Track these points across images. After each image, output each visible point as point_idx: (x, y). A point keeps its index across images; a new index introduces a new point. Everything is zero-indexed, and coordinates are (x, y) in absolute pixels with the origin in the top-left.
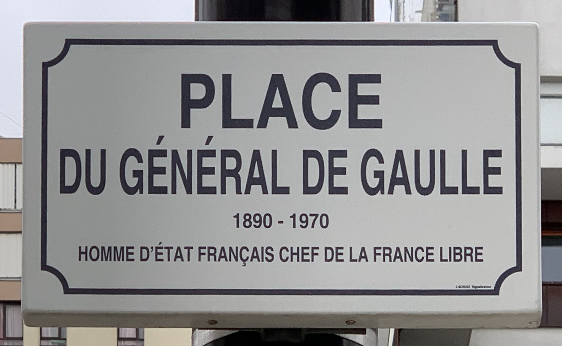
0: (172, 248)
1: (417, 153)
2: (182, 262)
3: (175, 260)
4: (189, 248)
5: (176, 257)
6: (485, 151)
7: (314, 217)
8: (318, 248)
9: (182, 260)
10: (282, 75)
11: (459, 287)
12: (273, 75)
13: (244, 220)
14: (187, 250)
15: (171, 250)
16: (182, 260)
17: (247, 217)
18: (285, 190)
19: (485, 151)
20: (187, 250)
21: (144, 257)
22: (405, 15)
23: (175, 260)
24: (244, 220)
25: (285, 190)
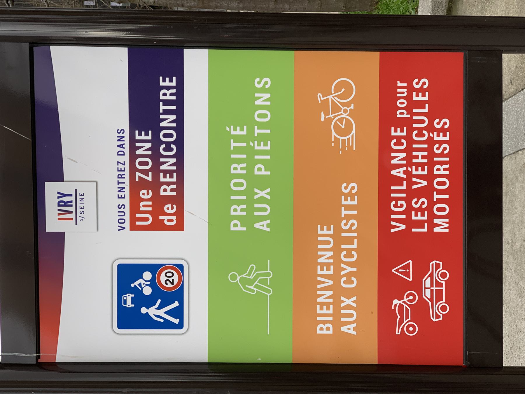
0: (118, 181)
1: (119, 216)
2: (125, 144)
3: (124, 148)
4: (119, 183)
5: (122, 147)
6: (125, 198)
7: (123, 163)
8: (118, 195)
9: (124, 144)
10: (403, 174)
11: (121, 190)
12: (267, 227)
13: (121, 174)
14: (119, 184)
15: (119, 182)
16: (124, 144)
17: (120, 176)
18: (118, 185)
19: (125, 198)
20: (119, 184)
21: (122, 153)
22: (144, 1)
23: (124, 148)
24: (121, 174)
25: (118, 185)
